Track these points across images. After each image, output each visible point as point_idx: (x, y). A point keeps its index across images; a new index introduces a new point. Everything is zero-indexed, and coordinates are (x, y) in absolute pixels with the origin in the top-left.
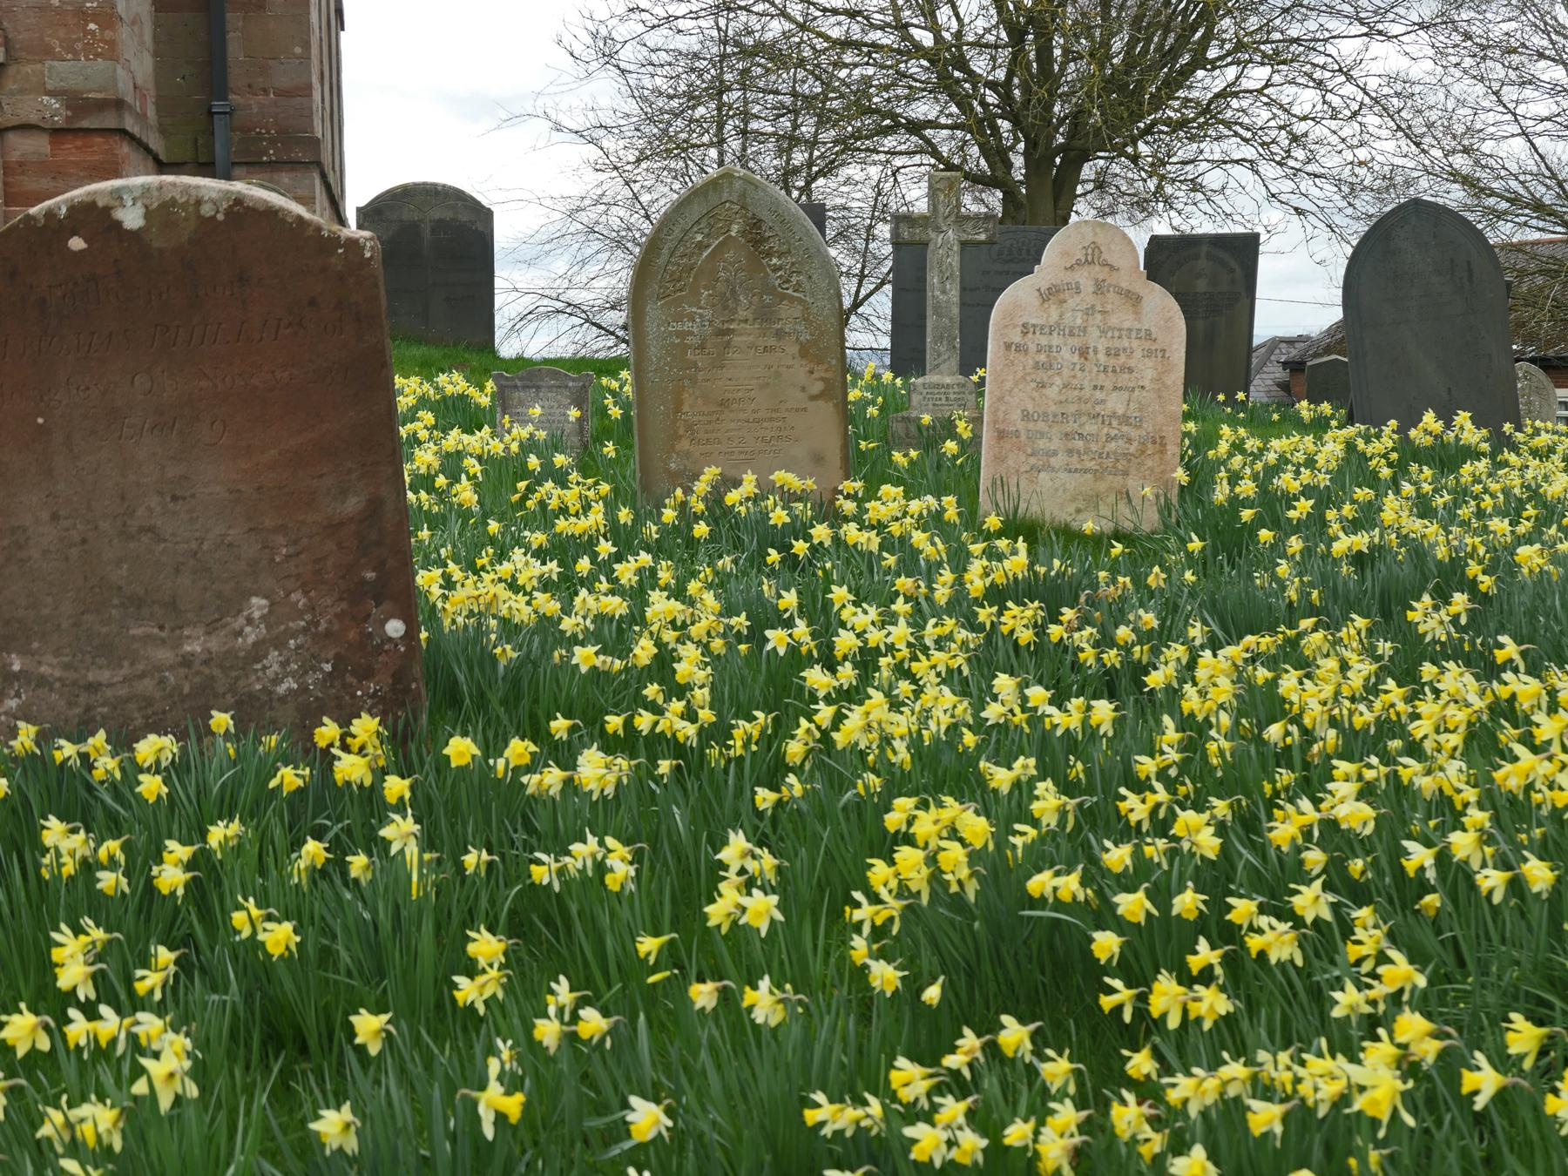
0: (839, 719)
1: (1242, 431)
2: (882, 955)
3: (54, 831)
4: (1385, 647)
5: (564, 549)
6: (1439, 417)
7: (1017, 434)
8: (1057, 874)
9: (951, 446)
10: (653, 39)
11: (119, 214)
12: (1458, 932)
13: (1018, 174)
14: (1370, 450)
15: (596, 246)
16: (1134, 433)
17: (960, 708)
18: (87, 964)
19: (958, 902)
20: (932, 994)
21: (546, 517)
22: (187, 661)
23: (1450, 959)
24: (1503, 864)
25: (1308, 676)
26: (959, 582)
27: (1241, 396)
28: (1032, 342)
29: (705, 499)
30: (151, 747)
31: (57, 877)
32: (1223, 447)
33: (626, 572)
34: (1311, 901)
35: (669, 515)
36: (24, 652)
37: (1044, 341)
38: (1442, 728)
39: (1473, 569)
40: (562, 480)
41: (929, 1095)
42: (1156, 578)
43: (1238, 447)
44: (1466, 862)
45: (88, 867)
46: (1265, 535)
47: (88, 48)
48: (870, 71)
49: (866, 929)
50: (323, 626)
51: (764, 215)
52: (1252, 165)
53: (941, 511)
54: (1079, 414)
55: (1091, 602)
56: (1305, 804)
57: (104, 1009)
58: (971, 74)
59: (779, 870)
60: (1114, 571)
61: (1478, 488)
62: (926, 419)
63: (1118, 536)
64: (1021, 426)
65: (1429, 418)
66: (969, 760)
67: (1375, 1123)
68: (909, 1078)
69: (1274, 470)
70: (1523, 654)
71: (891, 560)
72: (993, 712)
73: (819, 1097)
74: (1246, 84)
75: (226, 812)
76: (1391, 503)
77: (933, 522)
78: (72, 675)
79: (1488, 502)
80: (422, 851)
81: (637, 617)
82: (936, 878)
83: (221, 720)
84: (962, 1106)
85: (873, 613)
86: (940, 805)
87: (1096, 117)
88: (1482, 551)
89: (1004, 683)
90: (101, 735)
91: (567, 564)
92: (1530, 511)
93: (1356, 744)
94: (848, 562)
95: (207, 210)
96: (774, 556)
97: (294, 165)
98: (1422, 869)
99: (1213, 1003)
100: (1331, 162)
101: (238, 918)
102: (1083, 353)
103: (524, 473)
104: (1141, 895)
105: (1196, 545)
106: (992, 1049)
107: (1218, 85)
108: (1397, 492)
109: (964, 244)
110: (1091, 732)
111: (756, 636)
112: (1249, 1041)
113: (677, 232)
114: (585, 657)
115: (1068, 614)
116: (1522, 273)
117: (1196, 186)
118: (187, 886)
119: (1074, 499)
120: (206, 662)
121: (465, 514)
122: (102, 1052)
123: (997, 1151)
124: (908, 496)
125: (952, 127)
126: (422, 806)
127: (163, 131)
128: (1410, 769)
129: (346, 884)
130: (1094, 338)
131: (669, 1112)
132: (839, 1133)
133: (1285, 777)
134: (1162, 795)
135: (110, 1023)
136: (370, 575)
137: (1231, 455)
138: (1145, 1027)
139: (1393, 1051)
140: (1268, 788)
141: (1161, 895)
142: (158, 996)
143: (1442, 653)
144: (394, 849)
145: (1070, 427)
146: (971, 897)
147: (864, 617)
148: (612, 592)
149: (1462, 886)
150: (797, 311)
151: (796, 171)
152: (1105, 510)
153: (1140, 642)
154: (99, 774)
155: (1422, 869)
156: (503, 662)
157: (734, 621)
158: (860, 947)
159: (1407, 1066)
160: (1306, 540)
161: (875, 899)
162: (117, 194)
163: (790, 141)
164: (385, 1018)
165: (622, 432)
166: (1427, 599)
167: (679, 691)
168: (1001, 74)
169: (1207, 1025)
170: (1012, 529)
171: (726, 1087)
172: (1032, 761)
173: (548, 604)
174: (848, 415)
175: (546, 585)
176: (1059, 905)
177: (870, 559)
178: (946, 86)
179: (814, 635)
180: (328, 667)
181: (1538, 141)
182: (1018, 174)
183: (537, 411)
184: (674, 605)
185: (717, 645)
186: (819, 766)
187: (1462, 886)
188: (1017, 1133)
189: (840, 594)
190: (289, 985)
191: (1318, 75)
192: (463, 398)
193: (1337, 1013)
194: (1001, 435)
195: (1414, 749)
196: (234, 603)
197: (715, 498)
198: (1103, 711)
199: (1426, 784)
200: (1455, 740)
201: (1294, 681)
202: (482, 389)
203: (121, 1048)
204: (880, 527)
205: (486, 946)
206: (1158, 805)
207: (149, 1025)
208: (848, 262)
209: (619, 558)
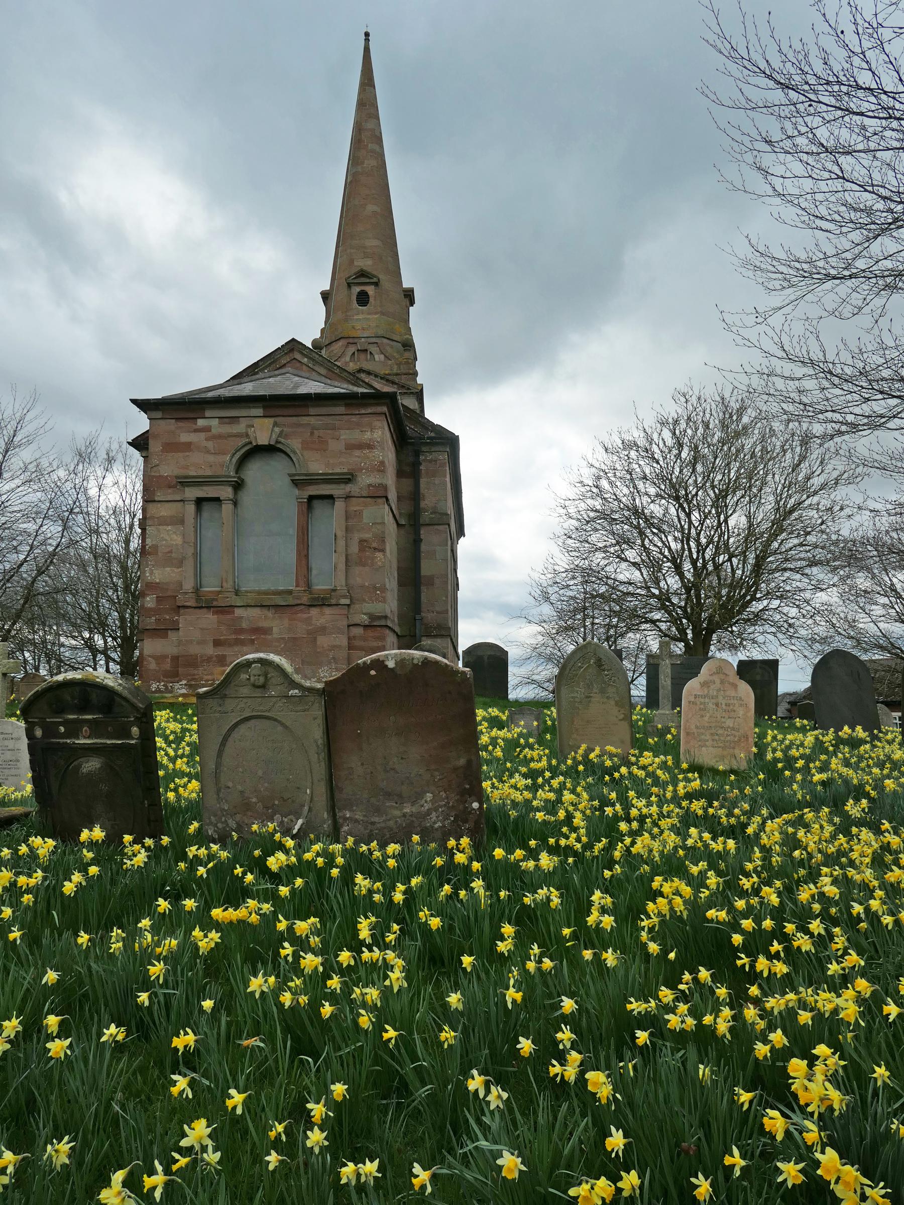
0: (633, 843)
1: (775, 732)
2: (653, 939)
3: (359, 879)
4: (837, 820)
5: (533, 774)
6: (850, 728)
7: (694, 733)
8: (718, 910)
9: (669, 736)
10: (561, 592)
11: (387, 663)
12: (875, 940)
13: (690, 636)
14: (824, 740)
15: (542, 660)
16: (737, 734)
17: (677, 841)
18: (370, 930)
19: (680, 918)
20: (672, 956)
21: (527, 761)
22: (404, 815)
23: (872, 950)
24: (892, 914)
25: (808, 831)
26: (675, 791)
27: (774, 717)
28: (698, 701)
29: (582, 756)
30: (392, 848)
31: (360, 895)
32: (769, 738)
33: (555, 783)
34: (816, 926)
35: (569, 762)
36: (351, 810)
37: (702, 700)
38: (862, 855)
39: (868, 788)
40: (532, 748)
41: (673, 1000)
42: (748, 790)
43: (774, 738)
44: (877, 911)
45: (370, 892)
46: (787, 773)
47: (377, 599)
48: (637, 603)
49: (646, 929)
50: (451, 804)
51: (602, 657)
52: (774, 634)
53: (666, 762)
54: (716, 727)
55: (725, 799)
56: (812, 886)
57: (375, 949)
58: (672, 603)
59: (613, 903)
60: (732, 788)
61: (867, 755)
62: (660, 726)
63: (732, 771)
64: (695, 731)
65: (846, 728)
66: (681, 862)
67: (849, 1024)
68: (666, 994)
69: (789, 748)
70: (892, 827)
71: (649, 781)
72: (690, 842)
73: (632, 1000)
74: (771, 606)
75: (417, 873)
76: (834, 761)
77: (664, 766)
78: (365, 819)
79: (871, 762)
80: (485, 891)
81: (559, 801)
82: (672, 909)
83: (416, 838)
84: (686, 1007)
85: (644, 801)
86: (673, 881)
87: (717, 618)
88: (871, 781)
89: (693, 831)
90: (375, 842)
91: (534, 779)
92: (888, 765)
93: (831, 860)
94: (634, 781)
95: (415, 662)
96: (607, 778)
97: (442, 636)
98: (859, 913)
99: (781, 968)
100: (803, 632)
101: (421, 914)
102: (717, 705)
103: (518, 745)
104: (750, 920)
105: (762, 776)
106: (696, 980)
107: (761, 607)
108: (836, 756)
109: (672, 664)
110: (727, 852)
111: (601, 809)
112: (796, 983)
113: (572, 663)
114: (540, 816)
115: (716, 804)
116: (876, 671)
117: (754, 641)
118: (404, 900)
119: (715, 757)
120: (411, 816)
121: (498, 759)
122: (373, 966)
123: (700, 1025)
124: (655, 757)
125: (666, 622)
126: (484, 875)
127: (399, 625)
128: (851, 872)
129: (458, 901)
131: (576, 1002)
132: (639, 1013)
133: (802, 872)
134: (755, 879)
135: (377, 953)
136: (467, 786)
137: (772, 742)
138: (753, 976)
139: (854, 993)
140: (796, 876)
141: (758, 921)
142: (393, 943)
143: (860, 823)
144: (475, 891)
145: (713, 731)
146: (685, 917)
147: (641, 803)
148: (550, 791)
149: (875, 922)
150: (614, 690)
151: (611, 636)
152: (726, 761)
153: (743, 815)
154: (374, 857)
155: (859, 913)
156: (512, 817)
157: (594, 803)
158: (644, 935)
159: (860, 1000)
160: (803, 775)
161: (649, 917)
162: (387, 656)
163: (609, 626)
164: (473, 958)
165: (552, 730)
166: (851, 801)
167: (575, 829)
168: (683, 604)
169: (779, 976)
170: (693, 768)
171: (596, 992)
172: (705, 863)
173: (527, 795)
174: (632, 725)
175: (527, 788)
176: (718, 922)
177: (642, 781)
178: (663, 607)
179: (623, 809)
180: (452, 819)
181: (879, 624)
182: (690, 636)
183: (522, 723)
184: (573, 796)
185: (588, 812)
186: (626, 860)
187: (875, 922)
188: (708, 1019)
189: (632, 794)
190: (438, 940)
191: (797, 603)
192: (497, 716)
193: (829, 973)
194: (688, 734)
195: (852, 863)
196: (420, 795)
197: (586, 755)
198: (731, 843)
199: (858, 878)
200: (868, 860)
201: (803, 833)
202: (504, 713)
203: (380, 962)
204: (644, 768)
205: (508, 930)
206: (754, 883)
207: (390, 955)
208: (629, 666)
209: (552, 778)
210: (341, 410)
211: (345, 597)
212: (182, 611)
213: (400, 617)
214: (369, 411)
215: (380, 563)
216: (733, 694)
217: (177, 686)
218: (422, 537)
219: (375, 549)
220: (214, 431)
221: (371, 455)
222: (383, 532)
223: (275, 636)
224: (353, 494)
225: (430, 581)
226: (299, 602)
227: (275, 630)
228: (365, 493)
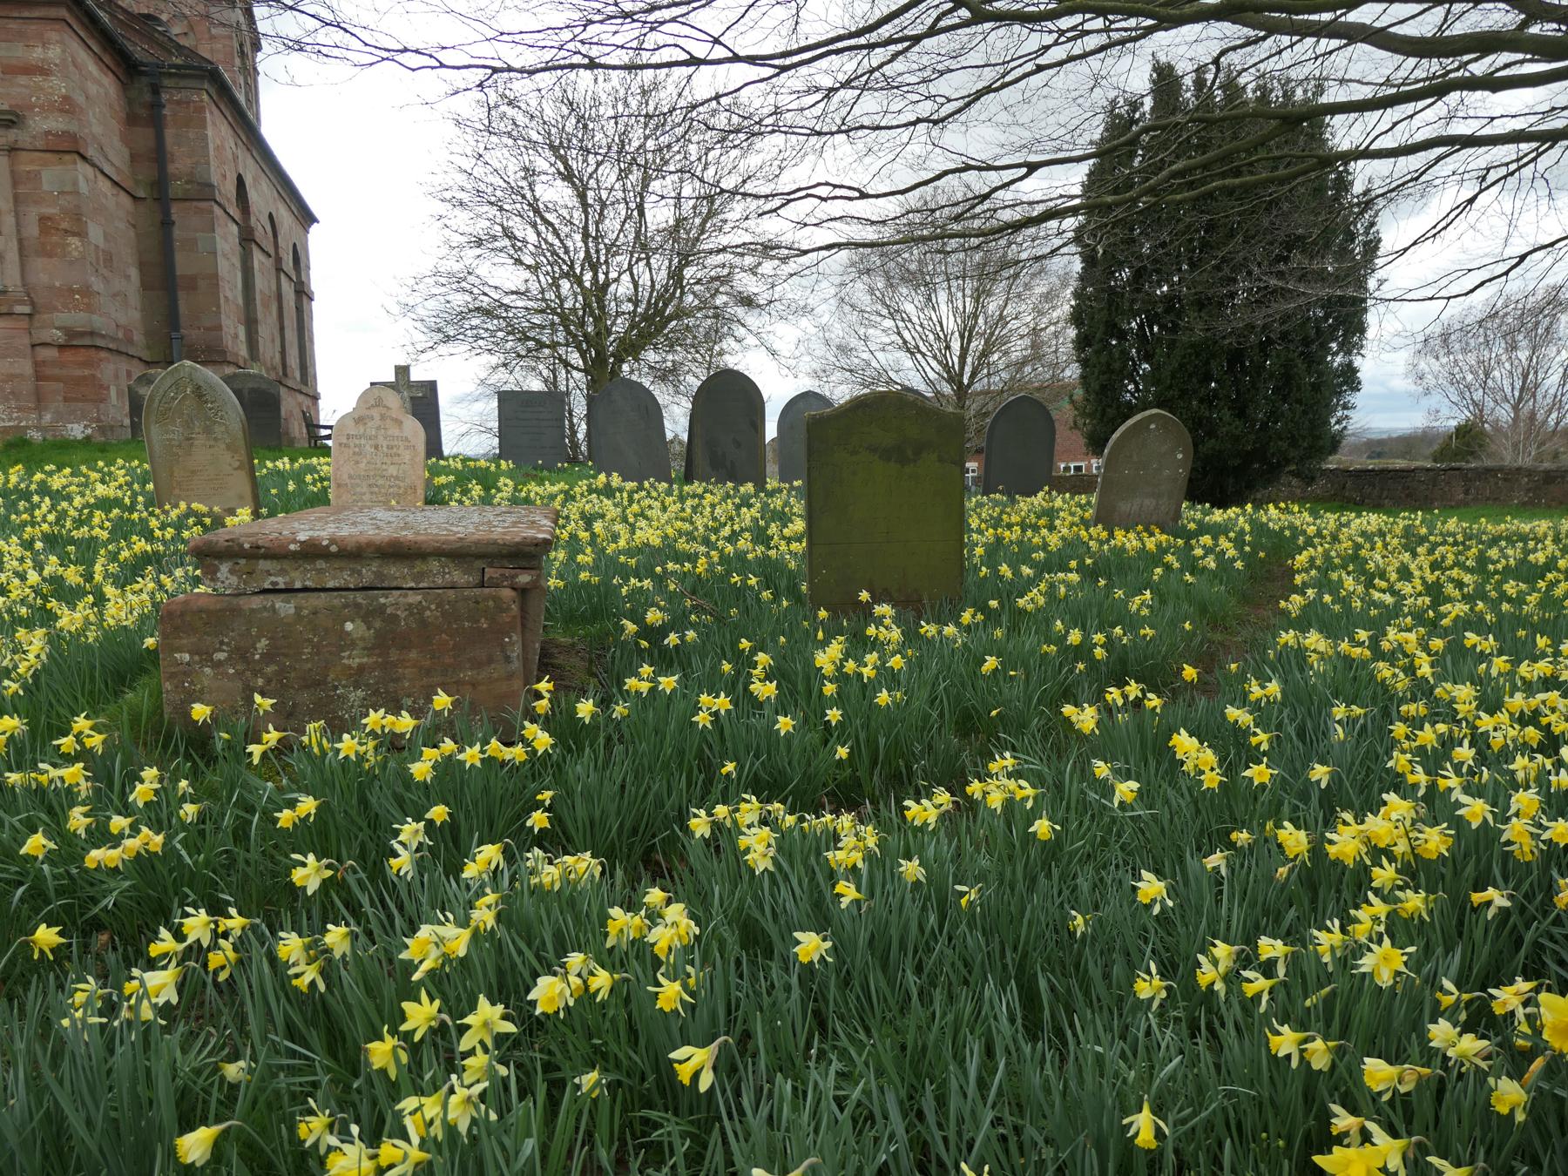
47: (76, 308)
102: (376, 447)
130: (381, 441)
145: (372, 481)
194: (339, 486)
213: (148, 334)
214: (36, 14)
215: (75, 254)
216: (396, 432)
218: (174, 217)
219: (66, 231)
221: (46, 85)
222: (78, 207)
224: (20, 145)
228: (39, 144)
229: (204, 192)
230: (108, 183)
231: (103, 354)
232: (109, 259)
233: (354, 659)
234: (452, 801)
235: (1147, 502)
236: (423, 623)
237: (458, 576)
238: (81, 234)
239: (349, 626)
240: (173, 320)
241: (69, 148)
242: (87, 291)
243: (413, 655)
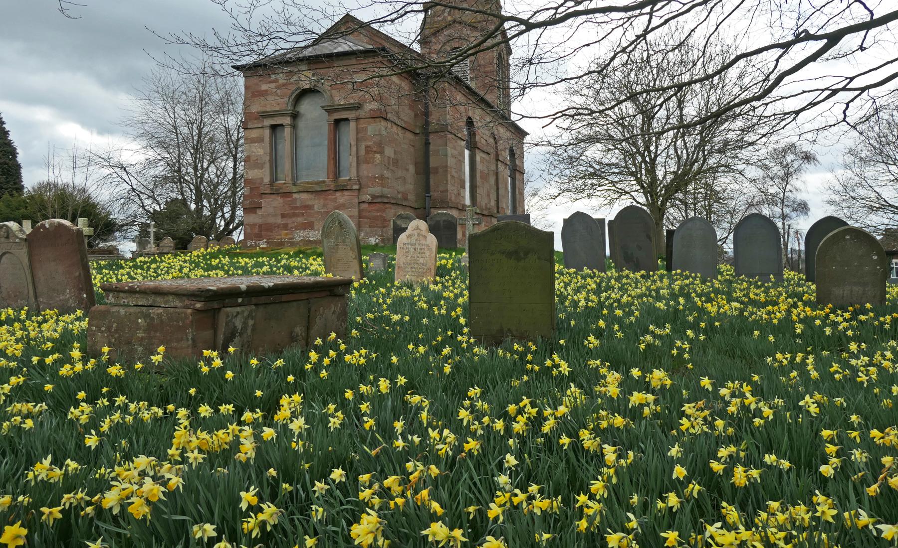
22: (60, 300)
102: (415, 249)
130: (418, 247)
194: (399, 267)
210: (354, 61)
211: (355, 184)
212: (263, 196)
217: (261, 242)
218: (430, 141)
220: (281, 82)
223: (316, 210)
225: (436, 170)
226: (328, 188)
227: (316, 207)
228: (368, 115)
229: (443, 129)
230: (400, 129)
231: (387, 206)
232: (396, 162)
233: (140, 334)
234: (691, 472)
235: (855, 289)
236: (162, 321)
237: (178, 303)
238: (381, 152)
239: (140, 321)
240: (427, 189)
241: (380, 116)
242: (382, 178)
243: (158, 334)
